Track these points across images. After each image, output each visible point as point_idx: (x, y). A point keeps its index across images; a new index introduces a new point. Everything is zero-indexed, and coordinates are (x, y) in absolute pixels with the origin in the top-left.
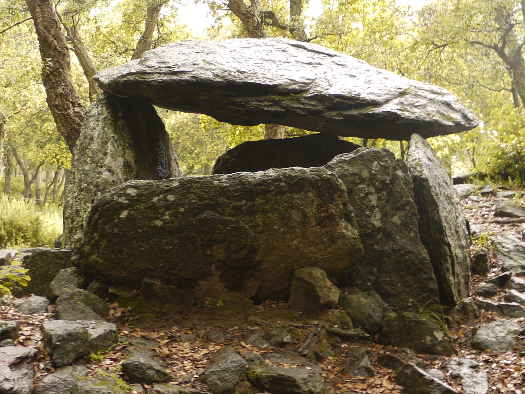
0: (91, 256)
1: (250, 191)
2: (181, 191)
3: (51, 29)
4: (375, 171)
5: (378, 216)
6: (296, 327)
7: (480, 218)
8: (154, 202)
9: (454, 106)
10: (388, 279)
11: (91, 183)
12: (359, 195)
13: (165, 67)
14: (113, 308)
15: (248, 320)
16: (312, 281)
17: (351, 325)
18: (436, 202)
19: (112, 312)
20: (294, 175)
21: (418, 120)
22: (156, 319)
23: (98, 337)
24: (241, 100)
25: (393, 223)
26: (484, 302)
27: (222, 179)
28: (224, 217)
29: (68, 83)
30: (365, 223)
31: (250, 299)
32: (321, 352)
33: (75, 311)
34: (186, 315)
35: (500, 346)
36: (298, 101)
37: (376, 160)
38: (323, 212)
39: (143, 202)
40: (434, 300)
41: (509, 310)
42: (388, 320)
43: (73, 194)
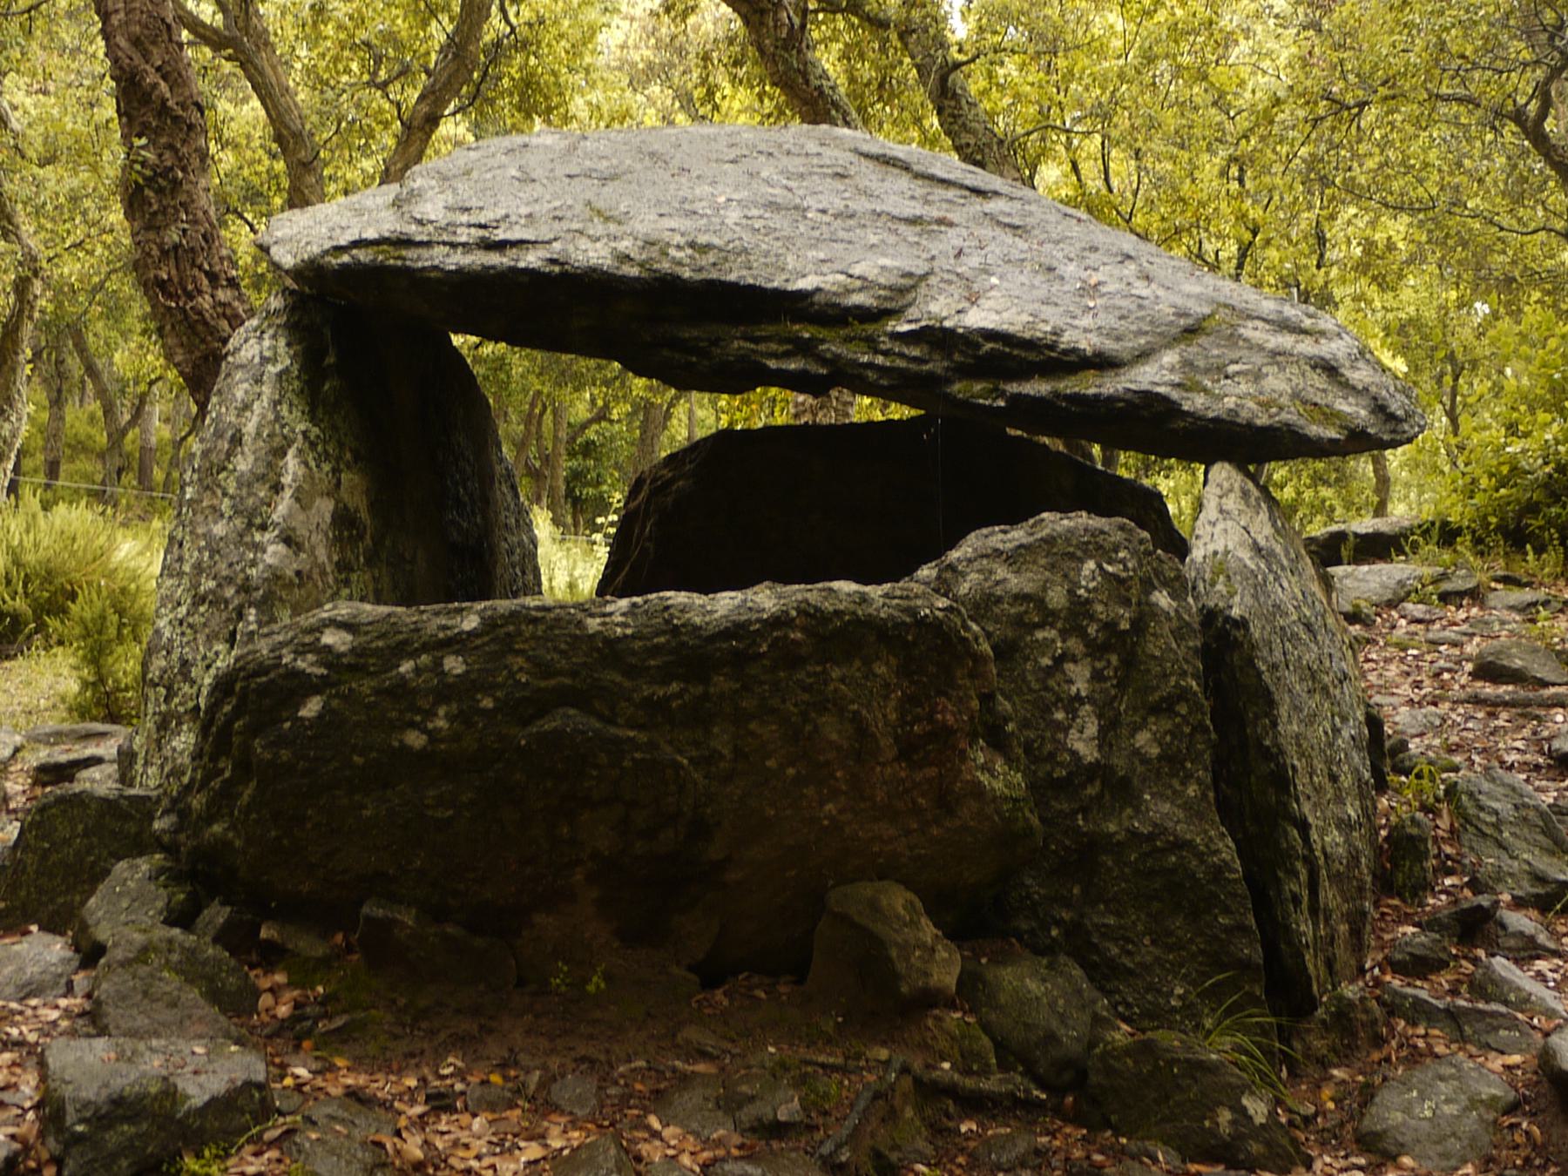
0: (210, 825)
1: (696, 653)
2: (484, 644)
3: (151, 47)
4: (1088, 590)
5: (1092, 729)
6: (823, 1066)
7: (1427, 682)
8: (402, 677)
9: (1348, 373)
10: (1111, 921)
11: (230, 580)
12: (1036, 661)
13: (470, 226)
14: (271, 990)
15: (679, 1039)
16: (878, 928)
17: (994, 1061)
18: (1269, 693)
19: (266, 1000)
20: (831, 609)
21: (1233, 423)
22: (398, 1030)
23: (208, 1104)
24: (695, 333)
25: (1136, 752)
26: (1405, 997)
27: (611, 614)
28: (613, 730)
29: (200, 214)
30: (1049, 747)
31: (690, 969)
32: (896, 1147)
33: (153, 1001)
34: (491, 1018)
35: (1439, 1148)
36: (871, 344)
37: (1091, 557)
38: (917, 719)
39: (370, 674)
40: (1250, 995)
41: (1478, 1026)
42: (1105, 1053)
43: (174, 608)
